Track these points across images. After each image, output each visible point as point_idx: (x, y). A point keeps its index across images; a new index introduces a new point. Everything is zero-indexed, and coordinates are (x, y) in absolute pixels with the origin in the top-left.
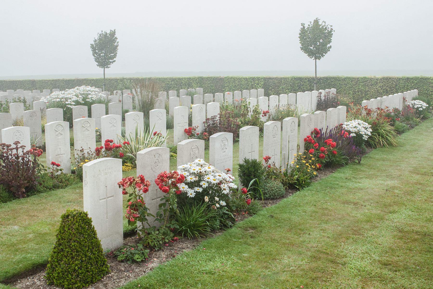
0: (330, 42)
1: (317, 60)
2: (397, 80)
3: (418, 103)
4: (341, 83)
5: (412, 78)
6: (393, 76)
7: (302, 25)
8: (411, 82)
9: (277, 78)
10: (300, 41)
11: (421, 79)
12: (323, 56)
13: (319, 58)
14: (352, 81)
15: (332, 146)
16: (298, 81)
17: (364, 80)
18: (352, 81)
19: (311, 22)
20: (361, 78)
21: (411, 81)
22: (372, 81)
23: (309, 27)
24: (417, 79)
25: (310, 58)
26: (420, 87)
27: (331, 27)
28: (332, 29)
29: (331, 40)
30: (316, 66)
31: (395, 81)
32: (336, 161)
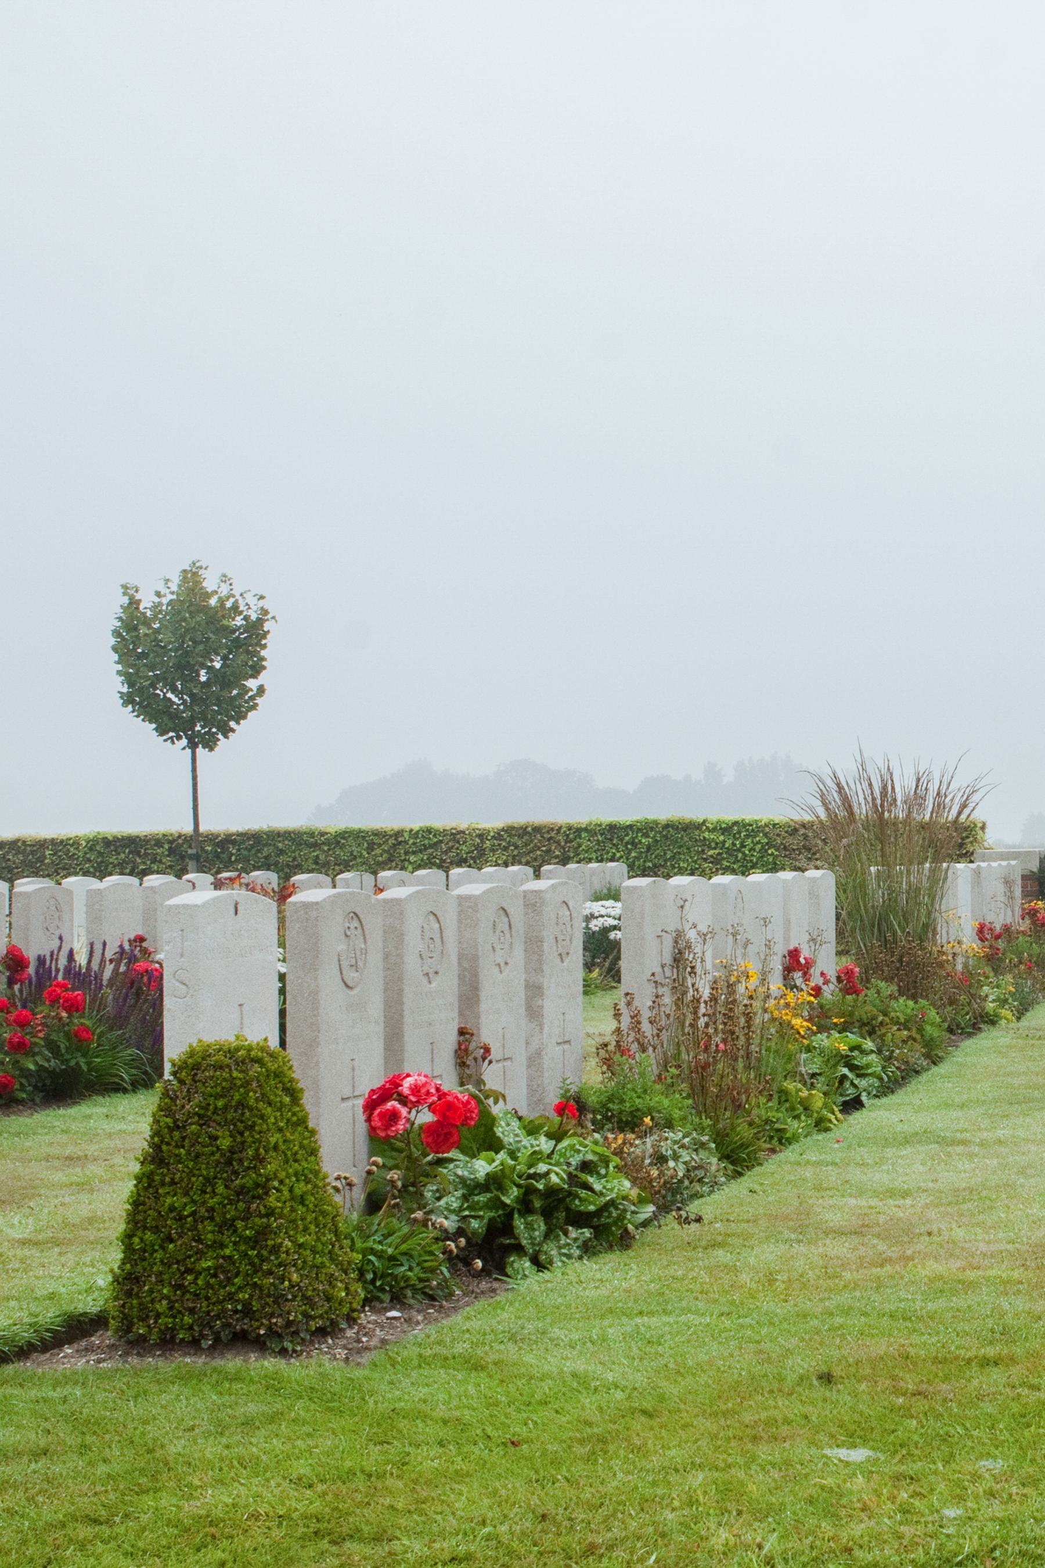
0: (257, 670)
1: (200, 751)
2: (568, 836)
3: (603, 912)
4: (322, 857)
5: (631, 827)
6: (553, 820)
7: (124, 594)
8: (627, 843)
9: (18, 840)
10: (120, 667)
11: (667, 826)
12: (226, 731)
13: (210, 744)
14: (371, 848)
15: (66, 1004)
16: (123, 856)
17: (426, 842)
18: (371, 848)
19: (167, 581)
20: (411, 831)
21: (627, 838)
22: (458, 842)
23: (160, 604)
24: (652, 829)
25: (165, 740)
26: (666, 861)
27: (261, 603)
28: (265, 612)
29: (263, 659)
30: (195, 778)
31: (558, 843)
32: (89, 1070)
